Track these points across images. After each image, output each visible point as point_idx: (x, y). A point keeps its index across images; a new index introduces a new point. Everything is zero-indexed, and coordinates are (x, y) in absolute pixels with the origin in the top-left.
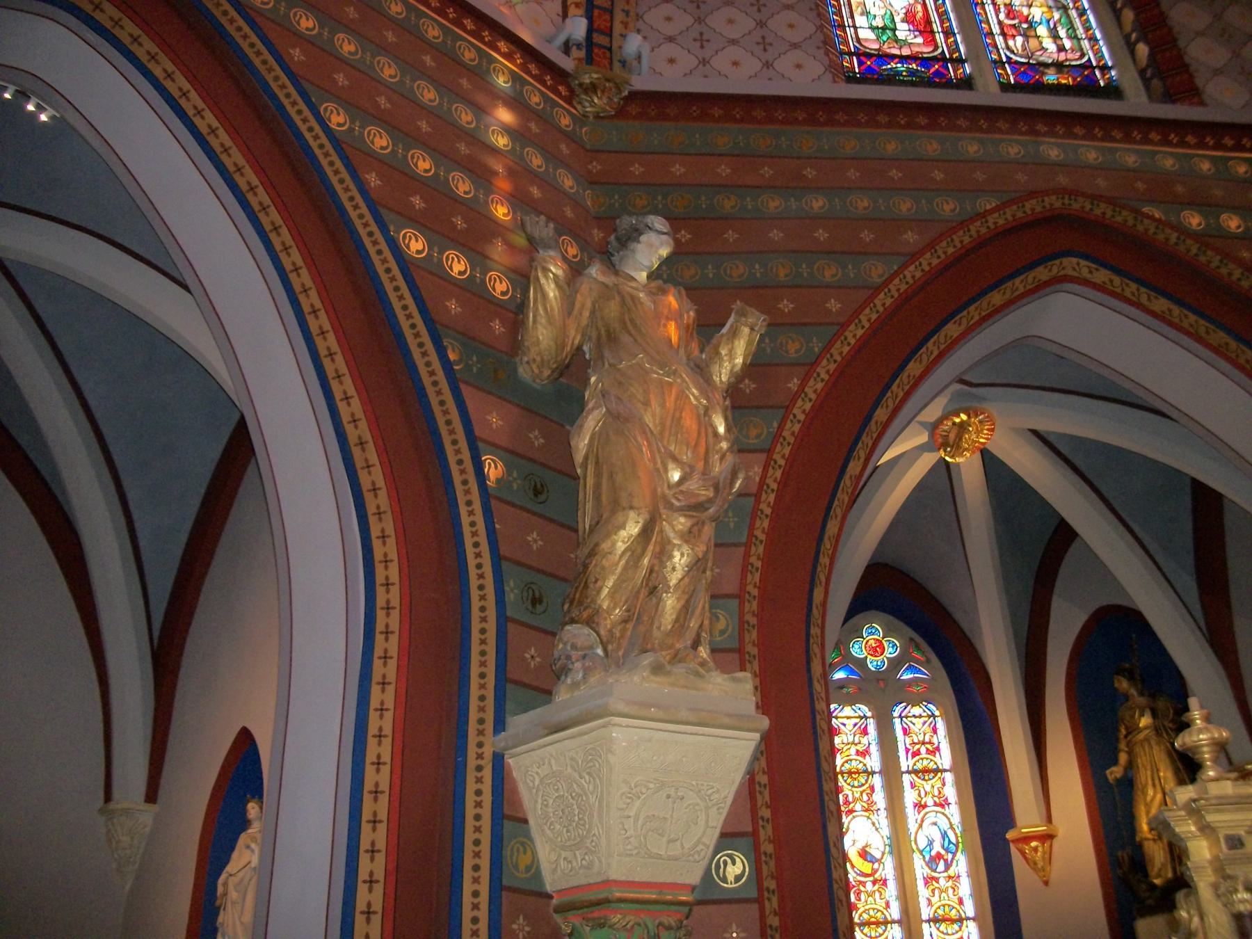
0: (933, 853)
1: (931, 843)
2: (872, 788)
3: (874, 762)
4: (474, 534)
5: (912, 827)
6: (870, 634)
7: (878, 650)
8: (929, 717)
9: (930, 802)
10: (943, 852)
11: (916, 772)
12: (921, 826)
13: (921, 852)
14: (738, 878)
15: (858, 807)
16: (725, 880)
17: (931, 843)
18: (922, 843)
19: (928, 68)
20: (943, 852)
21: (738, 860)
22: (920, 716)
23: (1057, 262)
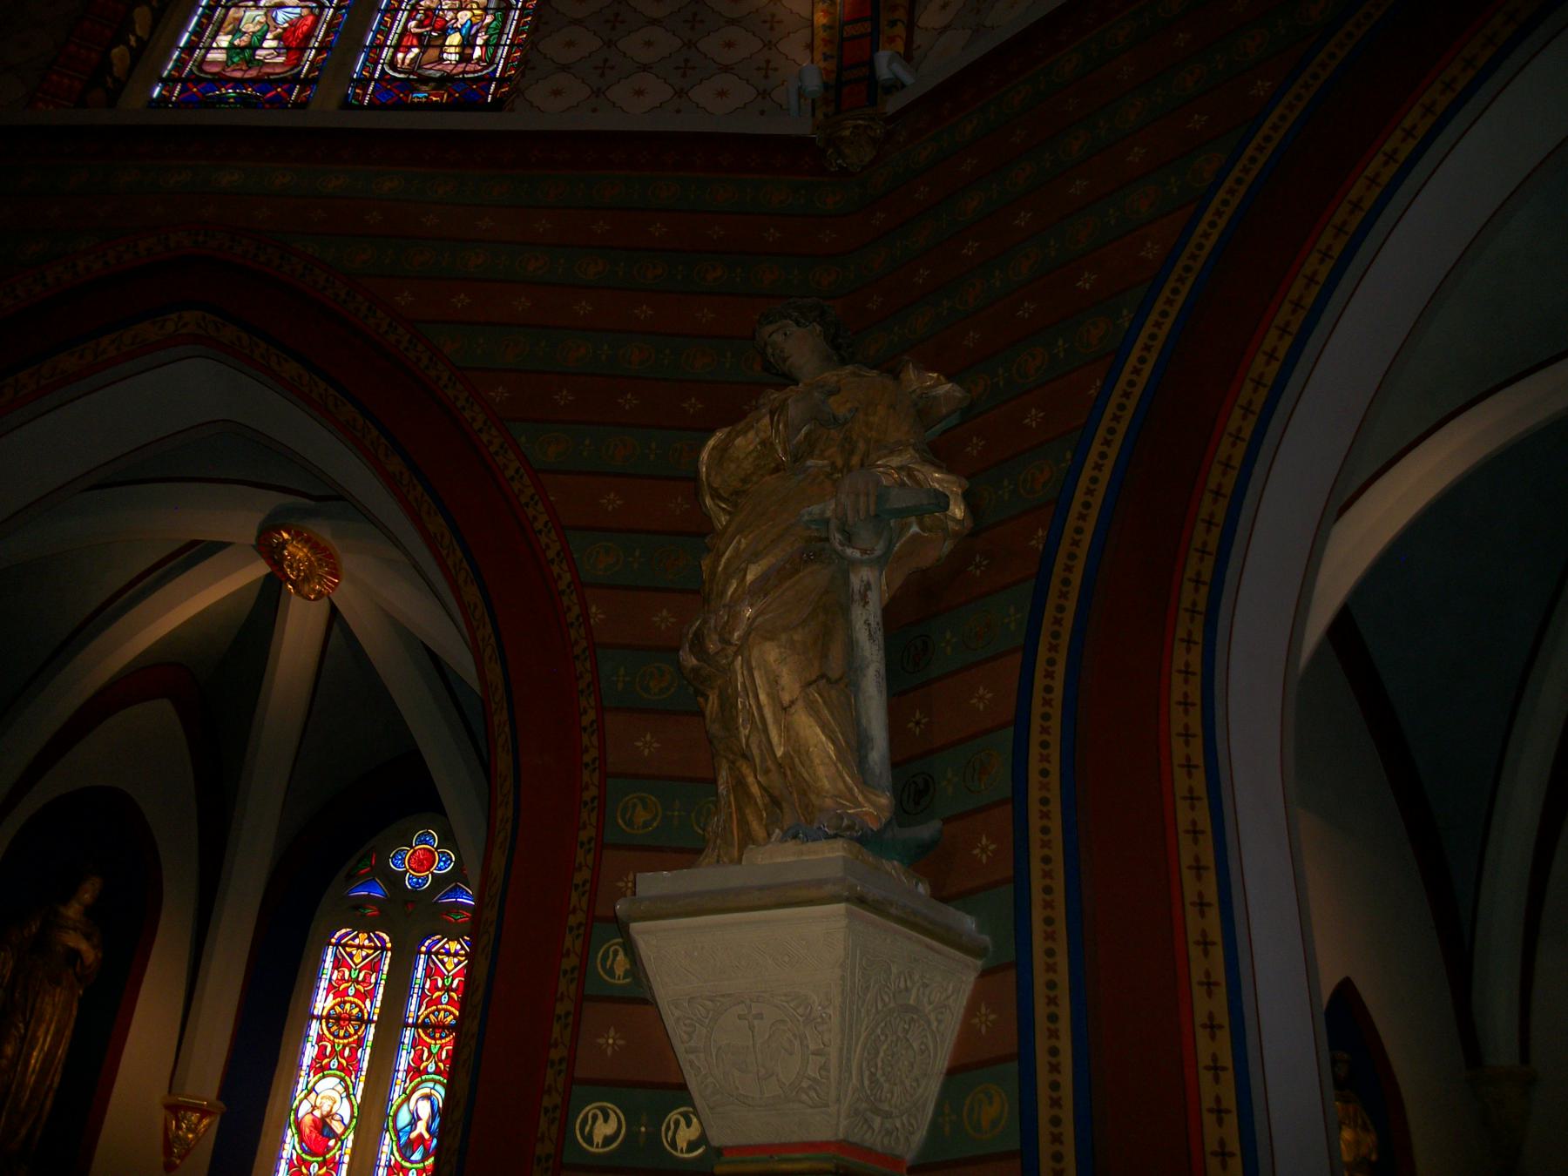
0: (413, 1135)
1: (415, 1119)
2: (360, 1042)
3: (373, 1007)
4: (1045, 730)
5: (397, 1096)
6: (421, 842)
7: (425, 862)
8: (375, 948)
9: (432, 1068)
10: (427, 1136)
11: (424, 1026)
12: (408, 1099)
13: (397, 1132)
14: (608, 1140)
15: (334, 1063)
16: (589, 1139)
17: (415, 1119)
18: (404, 1118)
19: (264, 93)
20: (427, 1136)
21: (612, 1116)
22: (456, 954)
23: (174, 316)
